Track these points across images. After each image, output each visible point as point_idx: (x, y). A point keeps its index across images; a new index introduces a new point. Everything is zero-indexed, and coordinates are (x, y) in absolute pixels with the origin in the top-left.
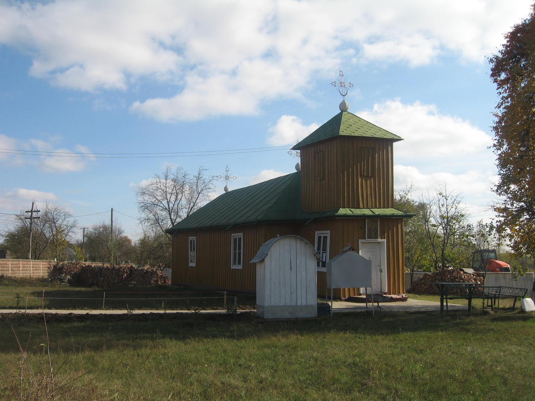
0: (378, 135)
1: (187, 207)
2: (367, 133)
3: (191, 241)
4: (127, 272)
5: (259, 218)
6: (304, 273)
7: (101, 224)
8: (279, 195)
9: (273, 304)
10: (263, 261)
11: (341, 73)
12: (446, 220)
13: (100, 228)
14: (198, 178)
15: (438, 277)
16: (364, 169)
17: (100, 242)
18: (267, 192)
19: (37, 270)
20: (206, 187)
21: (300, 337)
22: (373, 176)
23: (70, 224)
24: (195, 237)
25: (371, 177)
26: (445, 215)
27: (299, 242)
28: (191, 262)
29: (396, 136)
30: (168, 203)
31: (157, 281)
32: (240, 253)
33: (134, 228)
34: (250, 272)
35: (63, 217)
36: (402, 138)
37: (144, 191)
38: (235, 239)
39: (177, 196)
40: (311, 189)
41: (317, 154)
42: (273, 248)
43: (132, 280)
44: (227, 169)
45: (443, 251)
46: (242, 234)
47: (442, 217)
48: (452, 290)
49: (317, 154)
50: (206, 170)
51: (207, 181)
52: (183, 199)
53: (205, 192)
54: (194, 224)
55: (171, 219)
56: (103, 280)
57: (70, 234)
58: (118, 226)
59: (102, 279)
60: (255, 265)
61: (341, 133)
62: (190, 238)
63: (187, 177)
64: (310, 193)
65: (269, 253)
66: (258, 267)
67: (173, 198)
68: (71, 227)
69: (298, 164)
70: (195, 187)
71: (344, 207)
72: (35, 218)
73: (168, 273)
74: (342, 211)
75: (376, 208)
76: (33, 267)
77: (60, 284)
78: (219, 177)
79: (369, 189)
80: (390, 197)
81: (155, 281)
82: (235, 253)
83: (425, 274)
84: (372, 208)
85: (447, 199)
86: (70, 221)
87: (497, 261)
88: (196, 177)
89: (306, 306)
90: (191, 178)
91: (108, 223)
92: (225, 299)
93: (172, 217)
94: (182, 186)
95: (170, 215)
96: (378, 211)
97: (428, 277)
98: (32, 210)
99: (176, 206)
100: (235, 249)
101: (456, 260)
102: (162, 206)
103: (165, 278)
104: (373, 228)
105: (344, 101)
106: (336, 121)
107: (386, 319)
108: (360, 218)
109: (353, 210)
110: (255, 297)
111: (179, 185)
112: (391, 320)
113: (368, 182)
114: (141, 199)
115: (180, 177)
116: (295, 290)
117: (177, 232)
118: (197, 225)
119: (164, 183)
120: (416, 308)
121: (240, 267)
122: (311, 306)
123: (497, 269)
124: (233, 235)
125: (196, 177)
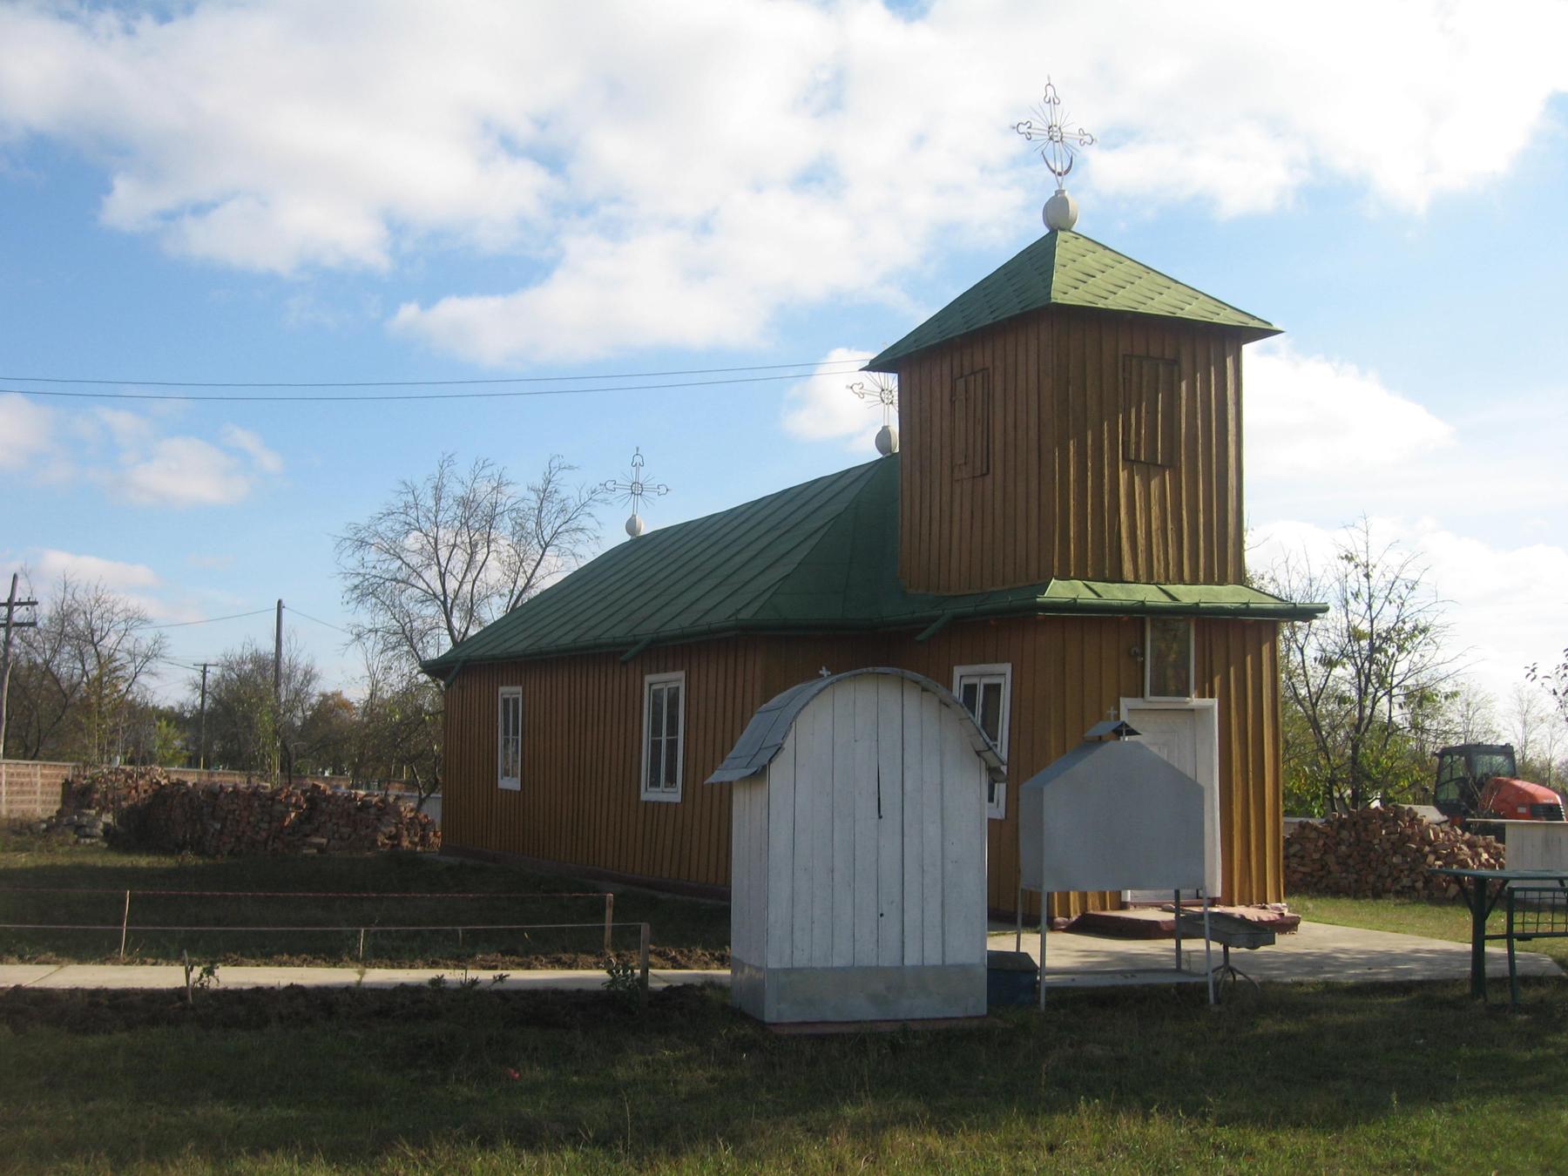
0: (1192, 311)
1: (506, 591)
2: (1150, 302)
3: (506, 701)
4: (297, 806)
6: (933, 830)
7: (247, 653)
9: (801, 960)
10: (760, 775)
12: (1364, 643)
13: (244, 662)
14: (544, 495)
15: (1344, 834)
17: (245, 707)
19: (23, 793)
20: (570, 522)
21: (935, 1142)
22: (1172, 463)
24: (519, 689)
25: (1163, 467)
26: (1365, 627)
27: (912, 699)
28: (506, 774)
29: (1254, 318)
30: (442, 576)
31: (395, 837)
32: (672, 745)
33: (346, 665)
34: (710, 818)
35: (123, 626)
36: (1276, 326)
37: (364, 534)
38: (657, 696)
39: (472, 555)
41: (961, 384)
42: (804, 723)
43: (316, 831)
44: (638, 460)
45: (1355, 748)
46: (681, 675)
47: (1355, 635)
48: (1397, 880)
49: (961, 384)
50: (570, 468)
51: (571, 505)
52: (492, 562)
53: (565, 541)
54: (519, 644)
55: (450, 629)
56: (221, 832)
57: (142, 678)
58: (303, 661)
59: (218, 826)
60: (727, 789)
61: (1057, 297)
62: (502, 690)
63: (508, 490)
66: (740, 800)
67: (460, 557)
68: (148, 658)
69: (885, 432)
71: (1064, 576)
72: (22, 625)
73: (433, 811)
74: (1059, 590)
75: (1181, 581)
76: (10, 784)
77: (77, 842)
78: (610, 485)
81: (390, 838)
82: (656, 746)
83: (1302, 826)
84: (1168, 581)
85: (1367, 576)
86: (144, 638)
87: (1518, 783)
88: (536, 491)
89: (943, 970)
90: (519, 493)
91: (268, 647)
93: (456, 623)
94: (491, 520)
96: (1189, 594)
97: (1313, 835)
98: (10, 600)
99: (467, 587)
100: (656, 730)
101: (1397, 776)
103: (424, 827)
105: (1060, 192)
107: (1268, 1026)
108: (1125, 617)
109: (1098, 586)
110: (727, 912)
111: (478, 520)
112: (1288, 1026)
113: (1154, 484)
114: (352, 563)
115: (483, 488)
116: (898, 899)
117: (467, 669)
118: (526, 644)
119: (429, 510)
120: (1354, 965)
121: (673, 795)
122: (964, 969)
123: (1522, 810)
124: (648, 678)
125: (536, 491)
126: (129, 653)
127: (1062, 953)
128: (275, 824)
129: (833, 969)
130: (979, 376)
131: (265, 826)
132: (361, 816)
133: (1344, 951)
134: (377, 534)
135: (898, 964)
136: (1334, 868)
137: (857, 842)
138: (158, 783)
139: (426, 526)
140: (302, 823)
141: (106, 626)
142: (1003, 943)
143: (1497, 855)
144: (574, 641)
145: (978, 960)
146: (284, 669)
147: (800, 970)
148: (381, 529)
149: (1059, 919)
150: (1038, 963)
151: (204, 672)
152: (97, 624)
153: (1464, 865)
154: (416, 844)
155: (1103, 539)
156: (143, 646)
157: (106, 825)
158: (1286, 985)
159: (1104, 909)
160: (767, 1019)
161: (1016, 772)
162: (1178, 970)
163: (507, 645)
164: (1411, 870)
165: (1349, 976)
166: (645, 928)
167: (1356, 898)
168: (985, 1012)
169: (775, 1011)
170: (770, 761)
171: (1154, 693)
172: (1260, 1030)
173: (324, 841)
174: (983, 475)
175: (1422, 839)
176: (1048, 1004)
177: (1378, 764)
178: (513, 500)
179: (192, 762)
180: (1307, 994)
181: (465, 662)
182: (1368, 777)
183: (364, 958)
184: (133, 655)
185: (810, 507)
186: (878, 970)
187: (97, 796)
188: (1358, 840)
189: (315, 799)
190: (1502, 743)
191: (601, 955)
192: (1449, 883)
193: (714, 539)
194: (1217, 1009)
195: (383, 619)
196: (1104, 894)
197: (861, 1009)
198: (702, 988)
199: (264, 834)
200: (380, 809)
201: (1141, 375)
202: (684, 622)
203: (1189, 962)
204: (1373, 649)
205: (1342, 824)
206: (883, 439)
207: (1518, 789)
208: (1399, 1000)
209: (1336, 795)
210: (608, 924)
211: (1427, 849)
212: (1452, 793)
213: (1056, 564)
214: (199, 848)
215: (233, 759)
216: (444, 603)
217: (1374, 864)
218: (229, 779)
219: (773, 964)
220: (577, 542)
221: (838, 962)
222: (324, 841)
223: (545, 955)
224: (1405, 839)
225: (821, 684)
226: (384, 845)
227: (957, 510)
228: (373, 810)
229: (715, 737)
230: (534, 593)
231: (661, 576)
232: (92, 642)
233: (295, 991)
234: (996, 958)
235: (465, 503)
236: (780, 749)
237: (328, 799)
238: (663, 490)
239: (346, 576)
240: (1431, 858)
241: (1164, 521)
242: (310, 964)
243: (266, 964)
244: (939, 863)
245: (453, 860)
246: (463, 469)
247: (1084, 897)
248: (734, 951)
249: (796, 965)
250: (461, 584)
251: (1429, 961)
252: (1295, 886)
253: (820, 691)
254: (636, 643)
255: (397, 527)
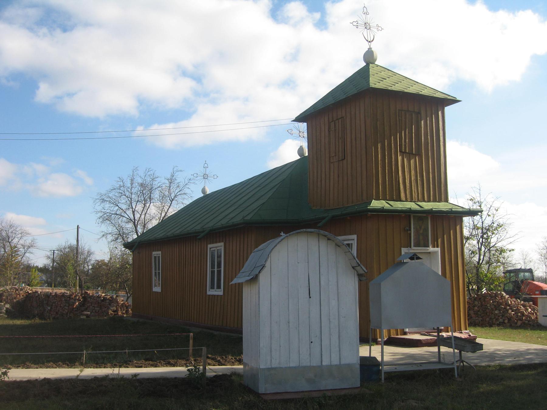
3: (155, 257)
5: (249, 218)
6: (334, 303)
8: (277, 187)
10: (254, 279)
11: (365, 11)
12: (480, 231)
14: (171, 181)
15: (476, 303)
16: (405, 141)
17: (66, 264)
18: (258, 186)
22: (419, 154)
23: (28, 244)
24: (160, 252)
25: (415, 155)
26: (479, 225)
27: (323, 244)
28: (155, 286)
29: (449, 96)
30: (133, 212)
31: (116, 311)
32: (219, 272)
33: (101, 248)
35: (20, 235)
36: (458, 99)
39: (145, 205)
40: (323, 176)
41: (332, 124)
43: (86, 310)
44: (206, 165)
46: (222, 244)
48: (497, 320)
49: (332, 124)
50: (181, 171)
51: (181, 185)
53: (179, 198)
54: (160, 235)
56: (50, 310)
57: (27, 255)
60: (240, 286)
61: (372, 85)
62: (154, 253)
63: (158, 180)
64: (323, 182)
65: (268, 264)
67: (139, 207)
68: (29, 247)
70: (167, 193)
71: (378, 199)
74: (376, 204)
75: (424, 201)
79: (413, 172)
80: (442, 186)
81: (114, 311)
82: (213, 272)
84: (418, 201)
86: (27, 240)
87: (534, 282)
89: (339, 367)
90: (162, 181)
92: (191, 351)
95: (136, 227)
96: (427, 206)
99: (143, 217)
102: (127, 216)
103: (127, 307)
104: (421, 232)
105: (370, 49)
106: (362, 75)
107: (484, 387)
108: (403, 215)
112: (494, 387)
113: (412, 161)
114: (99, 208)
117: (141, 246)
118: (163, 234)
119: (128, 188)
121: (220, 292)
122: (349, 366)
123: (537, 292)
124: (209, 246)
126: (22, 245)
127: (387, 354)
128: (70, 307)
129: (290, 368)
130: (340, 120)
131: (67, 308)
132: (103, 304)
133: (499, 350)
134: (109, 197)
135: (319, 364)
136: (473, 315)
137: (300, 310)
138: (28, 292)
139: (127, 194)
140: (81, 306)
141: (14, 235)
142: (364, 351)
143: (533, 309)
144: (181, 232)
145: (356, 361)
146: (80, 251)
147: (275, 369)
148: (110, 195)
149: (379, 340)
150: (379, 359)
151: (54, 253)
152: (10, 234)
153: (523, 314)
154: (124, 314)
155: (393, 183)
156: (28, 243)
157: (7, 308)
158: (484, 367)
159: (397, 335)
160: (260, 392)
161: (367, 276)
162: (439, 362)
163: (157, 235)
164: (503, 316)
165: (508, 362)
166: (204, 349)
167: (482, 327)
168: (359, 386)
169: (263, 388)
170: (259, 272)
171: (414, 246)
172: (481, 390)
173: (89, 313)
174: (342, 160)
175: (506, 304)
176: (385, 379)
177: (486, 276)
178: (160, 184)
179: (50, 285)
180: (492, 371)
181: (139, 243)
182: (483, 281)
183: (86, 363)
184: (24, 246)
185: (272, 178)
186: (310, 368)
187: (4, 298)
188: (482, 305)
189: (86, 297)
190: (528, 268)
191: (188, 360)
192: (517, 320)
193: (235, 192)
194: (459, 379)
195: (111, 229)
196: (397, 330)
197: (303, 386)
198: (231, 376)
199: (66, 311)
200: (110, 301)
201: (405, 118)
202: (224, 222)
203: (444, 358)
204: (483, 233)
205: (475, 299)
206: (300, 151)
207: (535, 284)
208: (533, 372)
209: (470, 288)
210: (191, 348)
211: (508, 307)
212: (510, 287)
213: (374, 194)
214: (41, 317)
215: (64, 285)
216: (134, 223)
217: (488, 314)
218: (60, 291)
219: (262, 366)
220: (184, 199)
221: (292, 365)
222: (89, 313)
223: (164, 360)
224: (499, 304)
225: (282, 238)
226: (111, 314)
227: (332, 174)
228: (107, 301)
229: (235, 263)
230: (167, 217)
231: (214, 207)
232: (9, 241)
233: (47, 381)
234: (363, 359)
235: (142, 185)
236: (264, 266)
237: (91, 297)
238: (215, 177)
239: (97, 212)
240: (510, 311)
241: (416, 176)
242: (59, 366)
243: (41, 367)
244: (337, 318)
245: (135, 320)
246: (141, 173)
247: (389, 332)
248: (244, 357)
249: (273, 366)
250: (141, 215)
251: (537, 354)
252: (472, 324)
253: (279, 243)
254: (203, 232)
255: (117, 194)
